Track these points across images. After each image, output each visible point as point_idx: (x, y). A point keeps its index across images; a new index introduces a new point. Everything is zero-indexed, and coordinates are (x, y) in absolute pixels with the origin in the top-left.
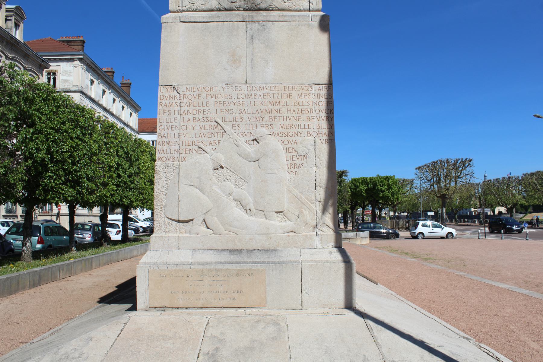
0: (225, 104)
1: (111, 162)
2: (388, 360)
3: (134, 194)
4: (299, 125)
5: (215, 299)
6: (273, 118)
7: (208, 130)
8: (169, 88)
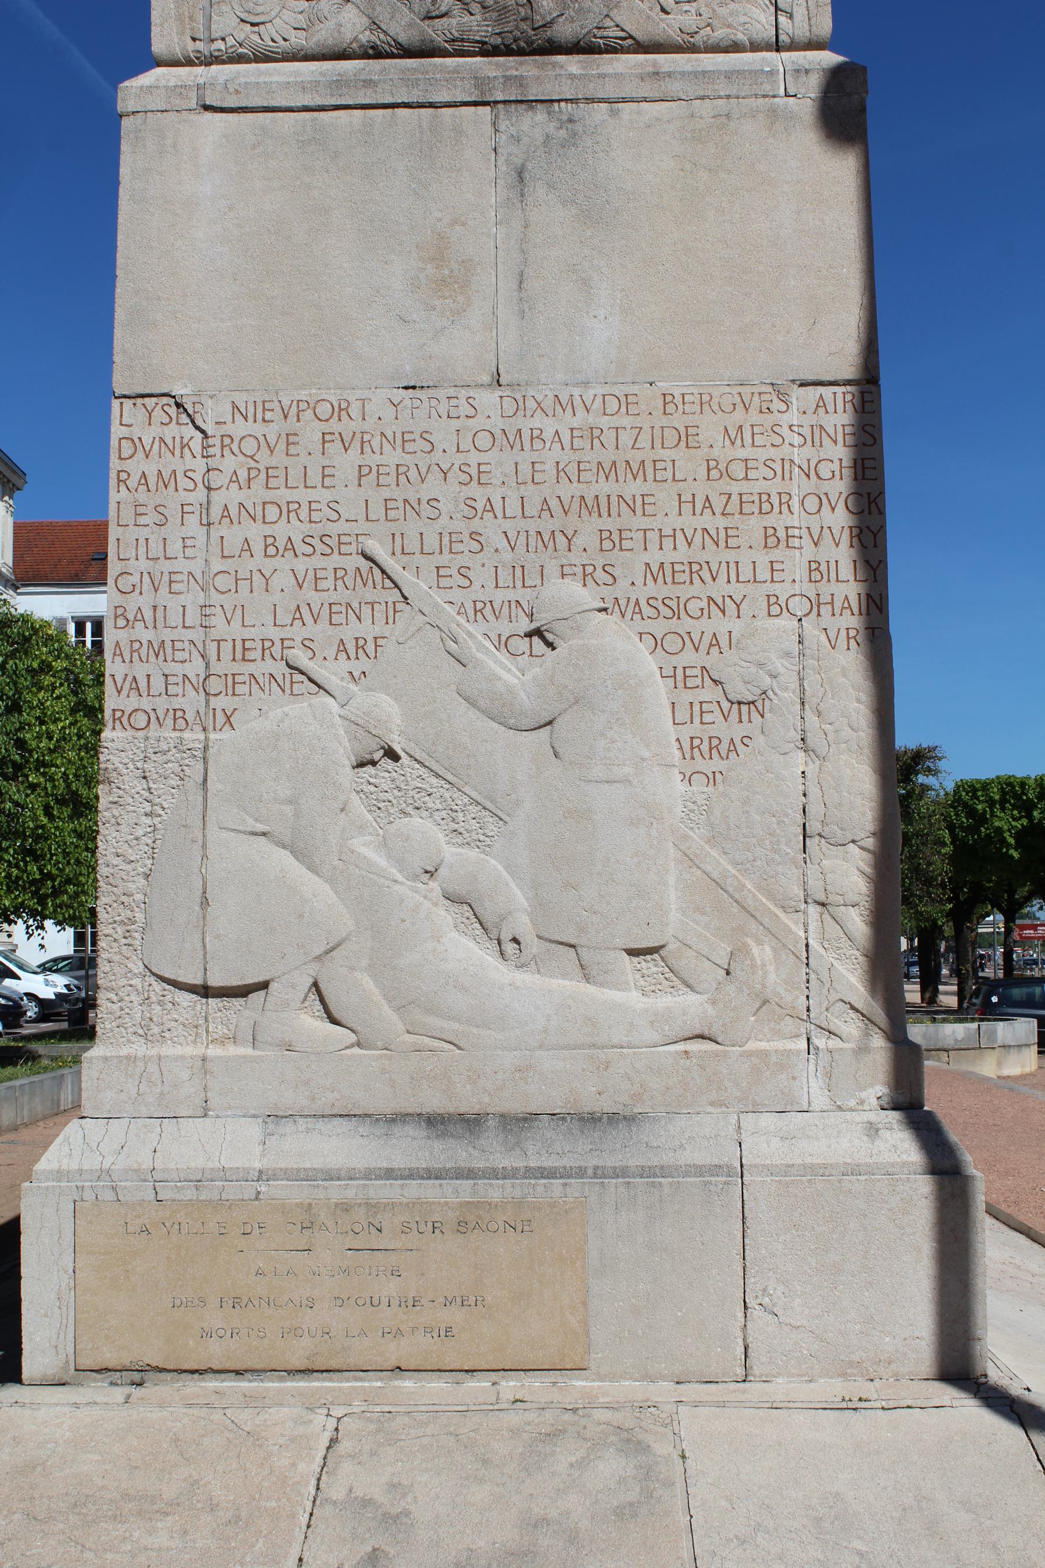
7: (331, 592)
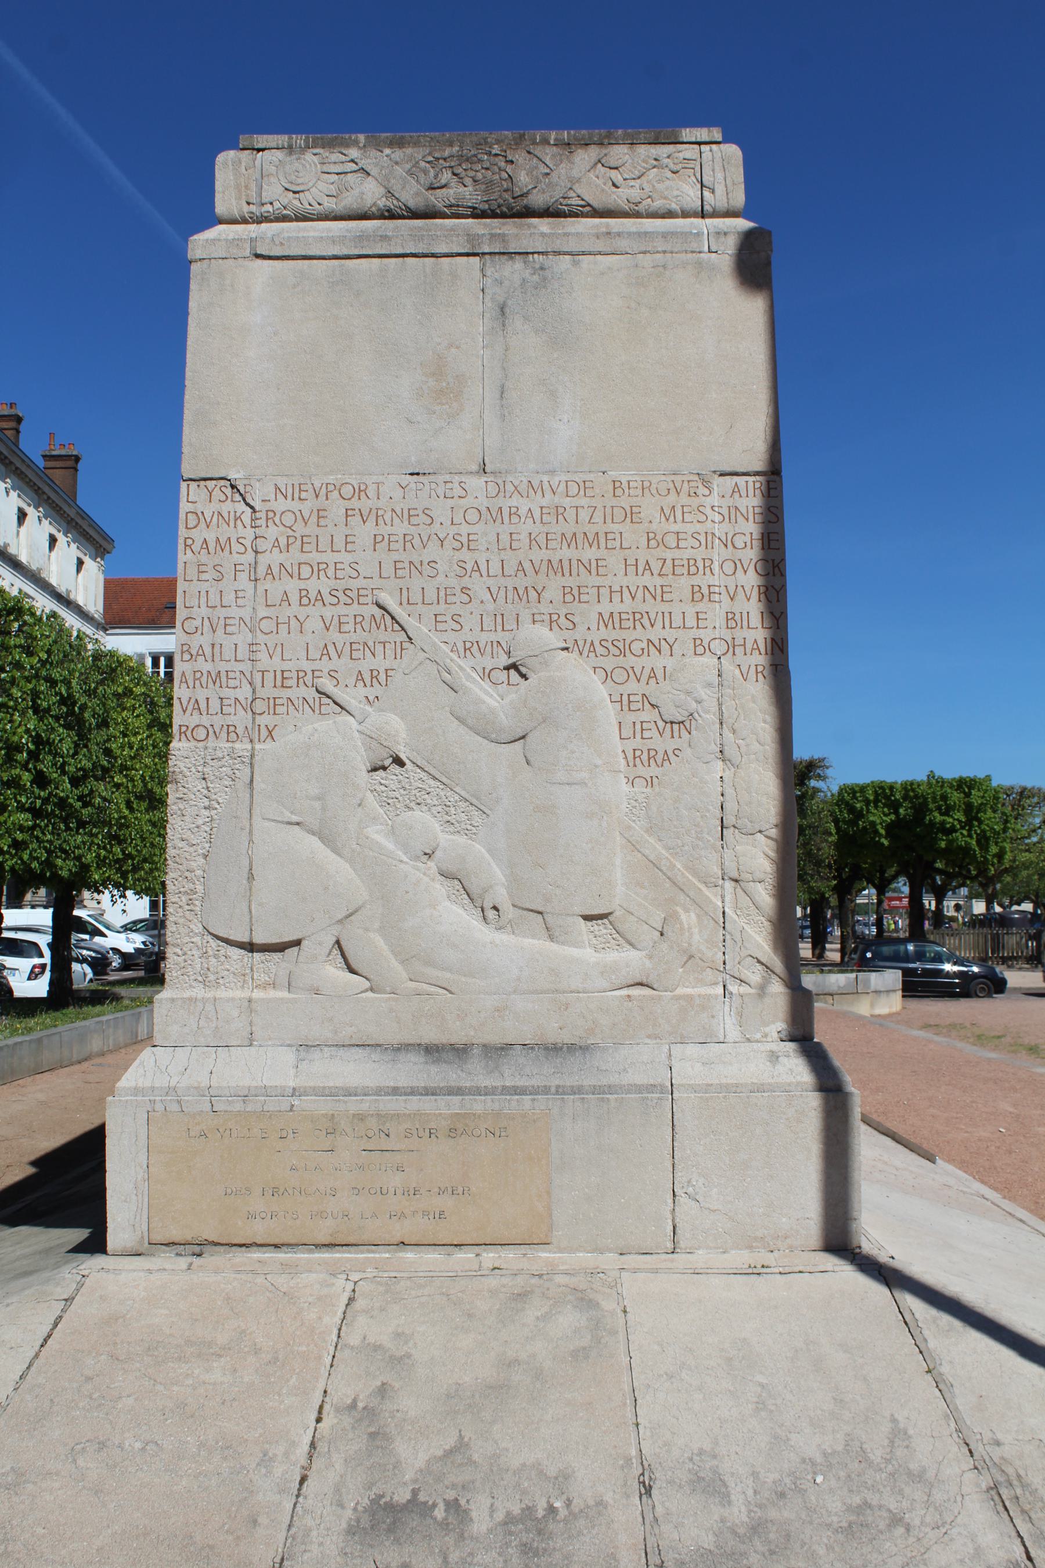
0: (408, 545)
1: (14, 734)
2: (979, 1437)
3: (92, 843)
4: (667, 615)
5: (375, 1215)
6: (575, 592)
7: (352, 633)
8: (217, 488)
